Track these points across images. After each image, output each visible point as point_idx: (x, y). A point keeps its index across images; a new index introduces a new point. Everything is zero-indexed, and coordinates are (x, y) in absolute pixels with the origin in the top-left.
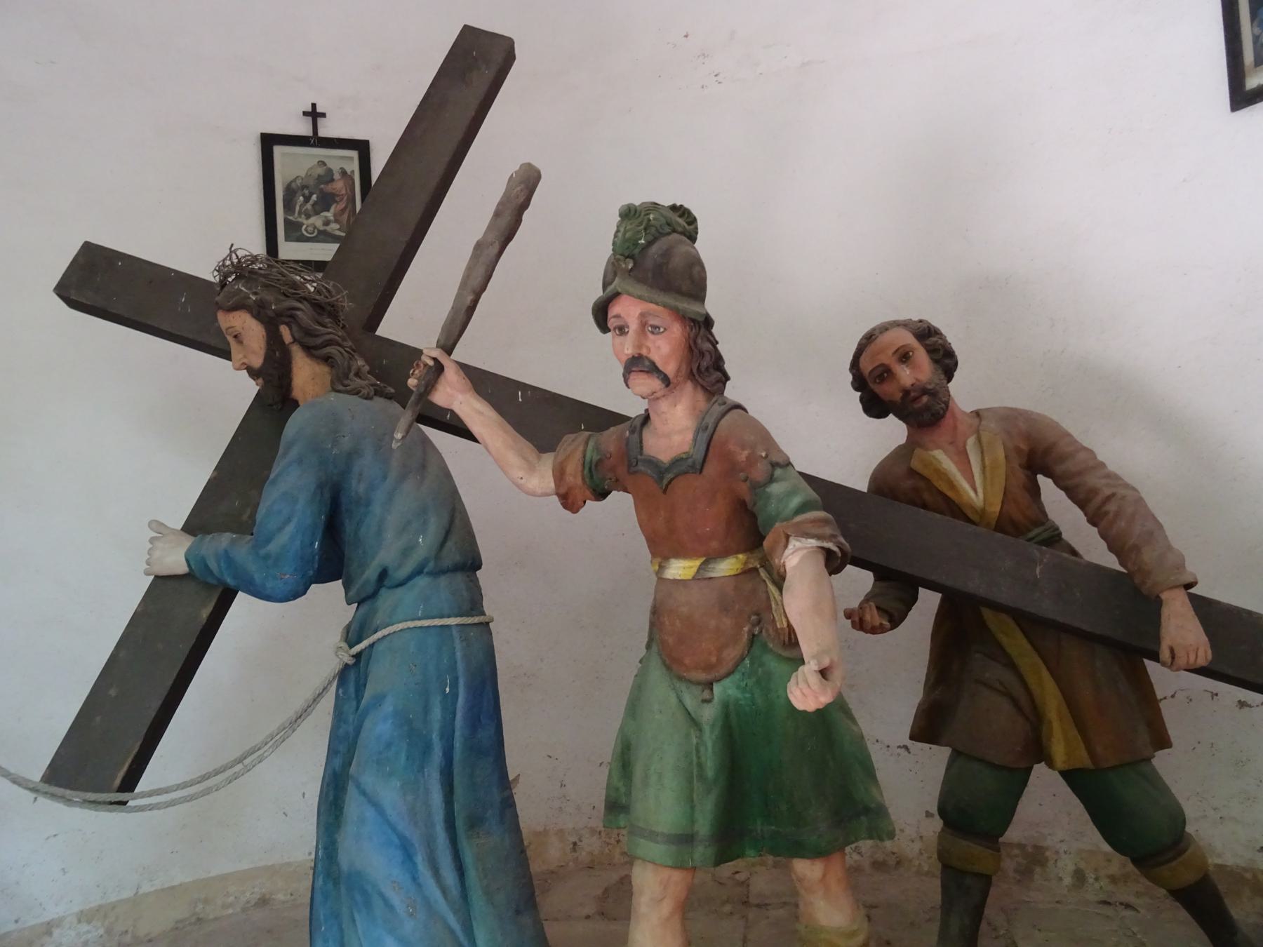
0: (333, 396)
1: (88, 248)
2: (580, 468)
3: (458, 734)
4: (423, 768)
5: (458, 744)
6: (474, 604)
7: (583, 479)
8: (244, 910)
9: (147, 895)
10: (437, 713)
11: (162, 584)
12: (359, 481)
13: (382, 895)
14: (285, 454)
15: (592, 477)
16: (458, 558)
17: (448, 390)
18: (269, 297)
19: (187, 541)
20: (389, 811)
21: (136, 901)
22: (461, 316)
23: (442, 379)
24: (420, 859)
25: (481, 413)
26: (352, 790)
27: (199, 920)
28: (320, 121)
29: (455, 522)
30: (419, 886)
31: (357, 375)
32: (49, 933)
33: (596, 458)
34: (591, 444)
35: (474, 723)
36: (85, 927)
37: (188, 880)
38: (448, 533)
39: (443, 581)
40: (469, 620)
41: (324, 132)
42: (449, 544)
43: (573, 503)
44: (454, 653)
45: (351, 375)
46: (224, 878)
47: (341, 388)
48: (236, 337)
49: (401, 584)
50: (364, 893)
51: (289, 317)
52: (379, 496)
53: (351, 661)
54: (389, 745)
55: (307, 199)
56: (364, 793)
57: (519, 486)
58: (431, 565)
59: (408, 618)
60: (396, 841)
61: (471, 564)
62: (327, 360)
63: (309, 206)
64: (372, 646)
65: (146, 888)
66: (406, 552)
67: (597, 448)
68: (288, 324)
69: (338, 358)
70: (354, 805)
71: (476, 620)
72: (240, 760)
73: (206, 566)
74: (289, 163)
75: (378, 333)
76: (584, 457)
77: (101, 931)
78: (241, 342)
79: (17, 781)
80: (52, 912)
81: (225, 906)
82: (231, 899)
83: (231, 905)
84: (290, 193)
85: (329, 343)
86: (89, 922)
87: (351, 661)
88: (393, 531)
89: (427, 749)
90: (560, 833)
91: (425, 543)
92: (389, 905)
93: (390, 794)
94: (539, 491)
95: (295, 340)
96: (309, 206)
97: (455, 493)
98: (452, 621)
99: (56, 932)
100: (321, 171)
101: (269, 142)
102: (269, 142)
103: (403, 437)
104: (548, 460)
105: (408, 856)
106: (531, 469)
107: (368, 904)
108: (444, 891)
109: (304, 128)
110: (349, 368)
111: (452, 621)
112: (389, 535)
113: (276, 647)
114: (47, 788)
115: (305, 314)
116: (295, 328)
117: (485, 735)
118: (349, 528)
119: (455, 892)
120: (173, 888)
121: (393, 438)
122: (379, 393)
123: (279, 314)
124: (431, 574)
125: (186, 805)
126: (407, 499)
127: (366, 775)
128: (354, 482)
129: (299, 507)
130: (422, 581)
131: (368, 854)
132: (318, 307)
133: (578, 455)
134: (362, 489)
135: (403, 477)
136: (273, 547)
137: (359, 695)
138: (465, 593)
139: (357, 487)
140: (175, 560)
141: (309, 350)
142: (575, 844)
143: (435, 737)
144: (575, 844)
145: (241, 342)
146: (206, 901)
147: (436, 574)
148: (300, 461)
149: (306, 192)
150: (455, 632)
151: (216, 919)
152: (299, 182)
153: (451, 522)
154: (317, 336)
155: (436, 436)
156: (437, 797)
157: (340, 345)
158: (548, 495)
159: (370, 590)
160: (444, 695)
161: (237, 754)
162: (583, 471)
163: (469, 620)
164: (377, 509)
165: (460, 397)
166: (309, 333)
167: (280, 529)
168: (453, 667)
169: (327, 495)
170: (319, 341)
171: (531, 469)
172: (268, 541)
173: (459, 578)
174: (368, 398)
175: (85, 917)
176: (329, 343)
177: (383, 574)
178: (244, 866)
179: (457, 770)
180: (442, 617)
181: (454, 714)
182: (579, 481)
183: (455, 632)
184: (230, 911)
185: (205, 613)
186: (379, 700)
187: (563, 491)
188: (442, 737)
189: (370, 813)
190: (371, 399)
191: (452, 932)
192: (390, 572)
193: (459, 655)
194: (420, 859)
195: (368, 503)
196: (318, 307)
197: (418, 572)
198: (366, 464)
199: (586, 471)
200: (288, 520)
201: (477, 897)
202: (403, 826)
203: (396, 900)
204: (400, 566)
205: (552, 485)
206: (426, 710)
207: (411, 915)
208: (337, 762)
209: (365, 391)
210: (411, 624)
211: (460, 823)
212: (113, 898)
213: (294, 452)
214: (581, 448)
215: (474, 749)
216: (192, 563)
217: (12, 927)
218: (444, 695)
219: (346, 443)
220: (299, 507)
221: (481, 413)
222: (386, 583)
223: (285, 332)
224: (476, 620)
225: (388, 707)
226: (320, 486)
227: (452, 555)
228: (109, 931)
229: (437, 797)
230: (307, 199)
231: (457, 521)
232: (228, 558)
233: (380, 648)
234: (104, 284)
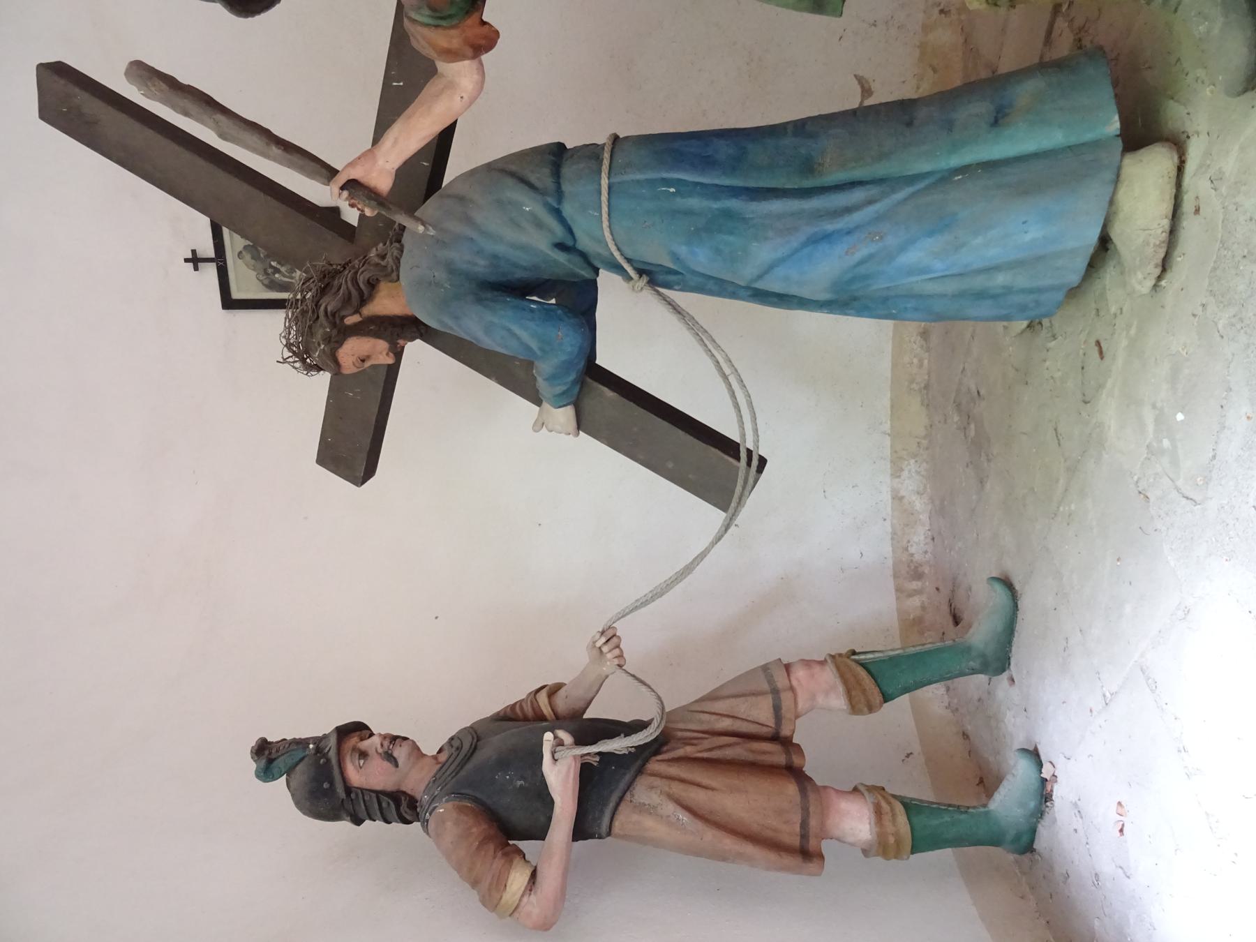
0: (404, 280)
1: (321, 460)
2: (440, 31)
3: (717, 181)
4: (744, 219)
5: (727, 182)
6: (591, 153)
7: (453, 27)
8: (928, 350)
9: (892, 427)
10: (694, 203)
11: (581, 424)
12: (476, 264)
13: (861, 262)
14: (451, 328)
15: (450, 16)
16: (546, 171)
17: (374, 175)
18: (319, 333)
19: (545, 405)
20: (779, 254)
21: (895, 435)
22: (295, 158)
23: (364, 180)
24: (829, 227)
25: (396, 141)
26: (759, 285)
27: (927, 387)
28: (200, 254)
29: (510, 170)
30: (858, 227)
31: (383, 257)
32: (902, 498)
33: (427, 12)
34: (413, 15)
35: (707, 163)
36: (905, 474)
37: (889, 395)
38: (523, 181)
39: (566, 187)
40: (606, 163)
41: (211, 253)
42: (533, 178)
43: (485, 37)
44: (638, 181)
45: (383, 263)
46: (895, 365)
47: (394, 274)
48: (363, 361)
49: (570, 231)
50: (852, 281)
51: (335, 319)
52: (490, 247)
53: (645, 279)
54: (718, 251)
55: (277, 271)
56: (760, 277)
57: (472, 101)
58: (550, 200)
59: (599, 228)
60: (806, 251)
61: (558, 152)
62: (373, 285)
63: (283, 269)
64: (629, 260)
65: (887, 427)
66: (539, 225)
67: (418, 9)
68: (343, 318)
69: (367, 275)
70: (773, 284)
71: (606, 155)
72: (725, 377)
73: (564, 393)
74: (246, 284)
75: (356, 224)
76: (427, 25)
77: (912, 461)
78: (369, 357)
79: (727, 527)
80: (886, 496)
81: (921, 365)
82: (915, 361)
83: (921, 361)
84: (272, 286)
85: (355, 281)
86: (902, 470)
87: (645, 279)
88: (523, 237)
89: (728, 214)
90: (926, 29)
91: (530, 205)
92: (870, 257)
93: (763, 252)
94: (476, 77)
95: (357, 311)
96: (283, 269)
97: (489, 167)
98: (605, 182)
99: (902, 493)
100: (248, 257)
101: (229, 303)
102: (229, 303)
103: (423, 224)
104: (442, 66)
105: (827, 237)
106: (451, 85)
107: (866, 277)
108: (870, 202)
109: (210, 271)
110: (377, 265)
111: (605, 182)
112: (523, 239)
113: (637, 337)
114: (731, 510)
115: (330, 303)
116: (343, 313)
117: (724, 150)
118: (519, 274)
119: (873, 191)
120: (892, 407)
121: (424, 236)
122: (399, 241)
123: (334, 325)
124: (560, 201)
125: (758, 421)
126: (489, 219)
127: (745, 273)
128: (477, 269)
129: (496, 320)
130: (568, 210)
131: (825, 268)
132: (323, 291)
133: (425, 31)
134: (482, 262)
135: (469, 221)
136: (534, 345)
137: (671, 272)
138: (582, 166)
139: (481, 267)
140: (566, 415)
141: (363, 301)
142: (942, 11)
143: (716, 205)
144: (942, 11)
145: (369, 357)
146: (912, 381)
147: (559, 194)
148: (456, 318)
149: (270, 271)
150: (615, 180)
151: (929, 374)
152: (261, 277)
153: (513, 175)
154: (350, 293)
155: (453, 170)
156: (776, 206)
157: (356, 273)
158: (481, 64)
159: (577, 259)
160: (678, 193)
161: (719, 380)
162: (445, 28)
163: (606, 163)
164: (500, 249)
165: (381, 162)
166: (347, 300)
167: (519, 339)
168: (652, 183)
169: (489, 295)
170: (354, 293)
171: (451, 85)
172: (528, 348)
173: (568, 171)
174: (401, 250)
175: (896, 473)
176: (355, 281)
177: (561, 246)
178: (888, 347)
179: (752, 183)
180: (600, 193)
181: (697, 184)
182: (453, 32)
183: (615, 180)
184: (926, 362)
185: (609, 393)
186: (676, 257)
187: (469, 52)
188: (716, 199)
189: (780, 271)
190: (402, 246)
191: (913, 195)
192: (557, 241)
193: (639, 176)
194: (829, 227)
195: (495, 256)
196: (323, 291)
197: (557, 213)
198: (461, 257)
199: (444, 23)
200: (509, 330)
201: (881, 170)
202: (796, 240)
203: (863, 252)
204: (551, 231)
205: (467, 62)
206: (689, 213)
207: (881, 238)
208: (742, 293)
209: (396, 253)
210: (605, 224)
211: (808, 183)
212: (888, 452)
213: (450, 322)
214: (419, 28)
215: (735, 165)
216: (1109, 175)
217: (888, 524)
218: (678, 193)
219: (441, 275)
220: (496, 320)
221: (396, 141)
222: (570, 243)
223: (351, 320)
224: (606, 155)
225: (683, 250)
226: (479, 300)
227: (541, 177)
228: (914, 456)
229: (776, 206)
230: (277, 271)
231: (513, 168)
232: (552, 378)
233: (630, 254)
234: (353, 444)
